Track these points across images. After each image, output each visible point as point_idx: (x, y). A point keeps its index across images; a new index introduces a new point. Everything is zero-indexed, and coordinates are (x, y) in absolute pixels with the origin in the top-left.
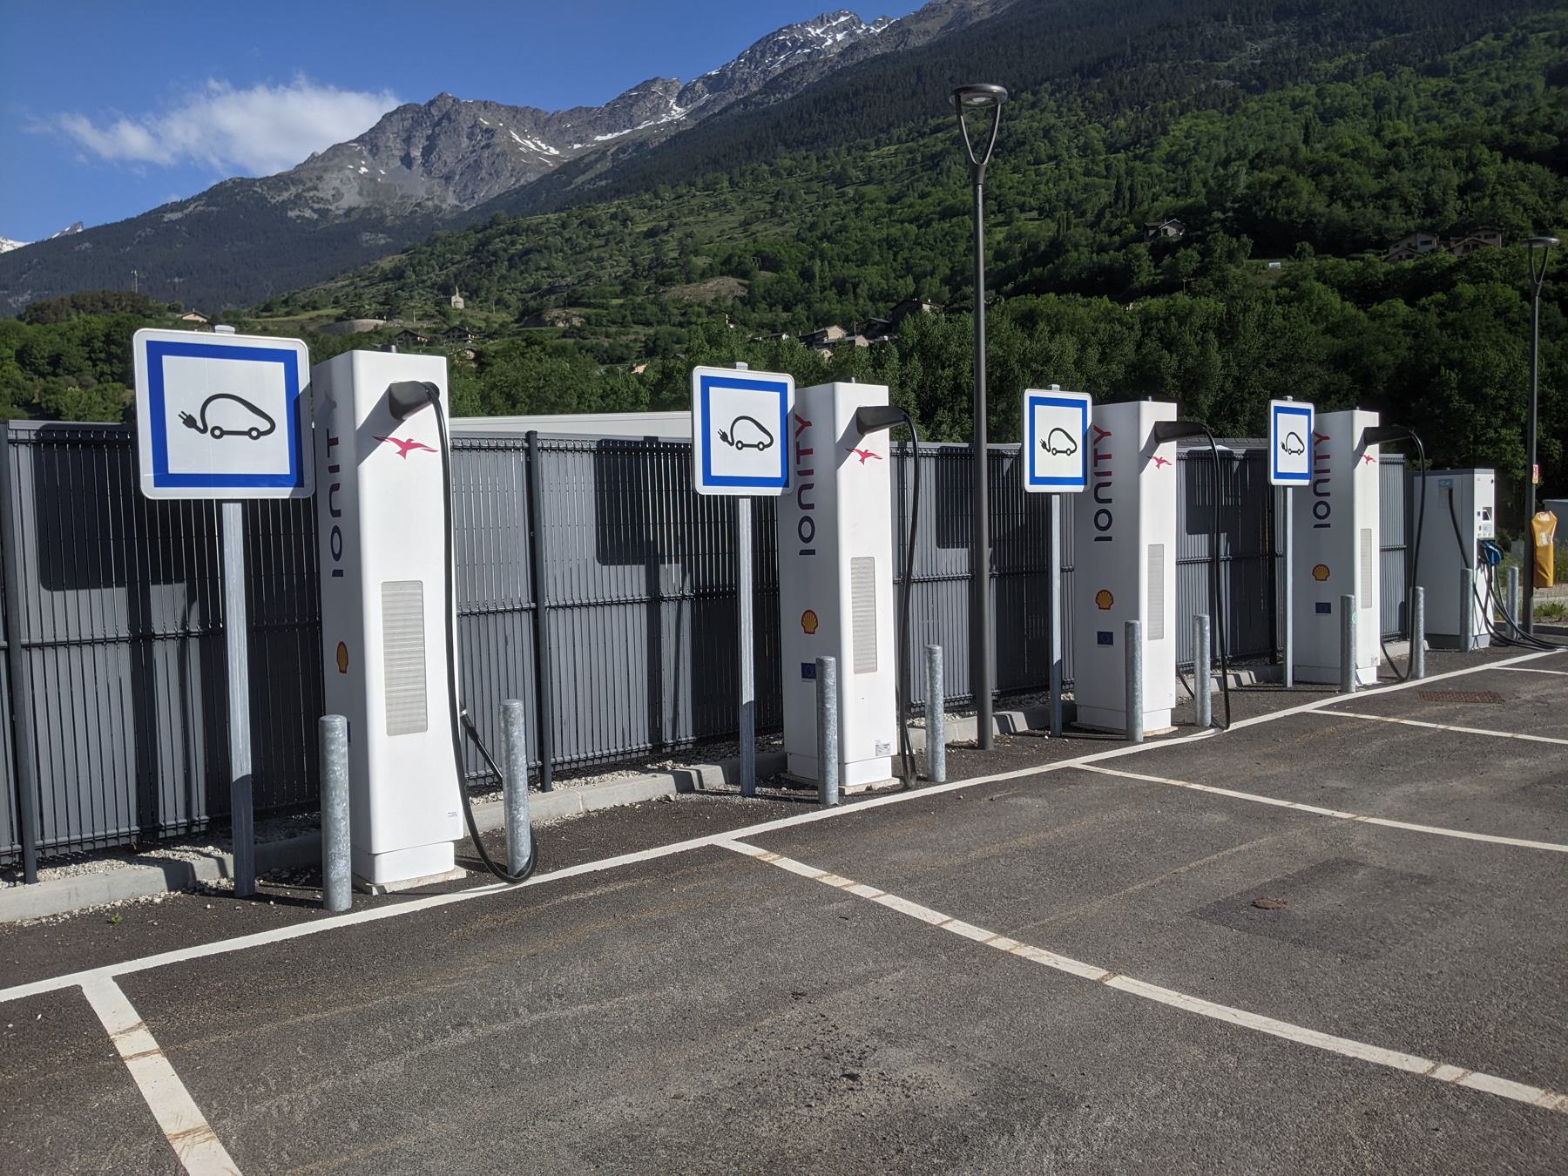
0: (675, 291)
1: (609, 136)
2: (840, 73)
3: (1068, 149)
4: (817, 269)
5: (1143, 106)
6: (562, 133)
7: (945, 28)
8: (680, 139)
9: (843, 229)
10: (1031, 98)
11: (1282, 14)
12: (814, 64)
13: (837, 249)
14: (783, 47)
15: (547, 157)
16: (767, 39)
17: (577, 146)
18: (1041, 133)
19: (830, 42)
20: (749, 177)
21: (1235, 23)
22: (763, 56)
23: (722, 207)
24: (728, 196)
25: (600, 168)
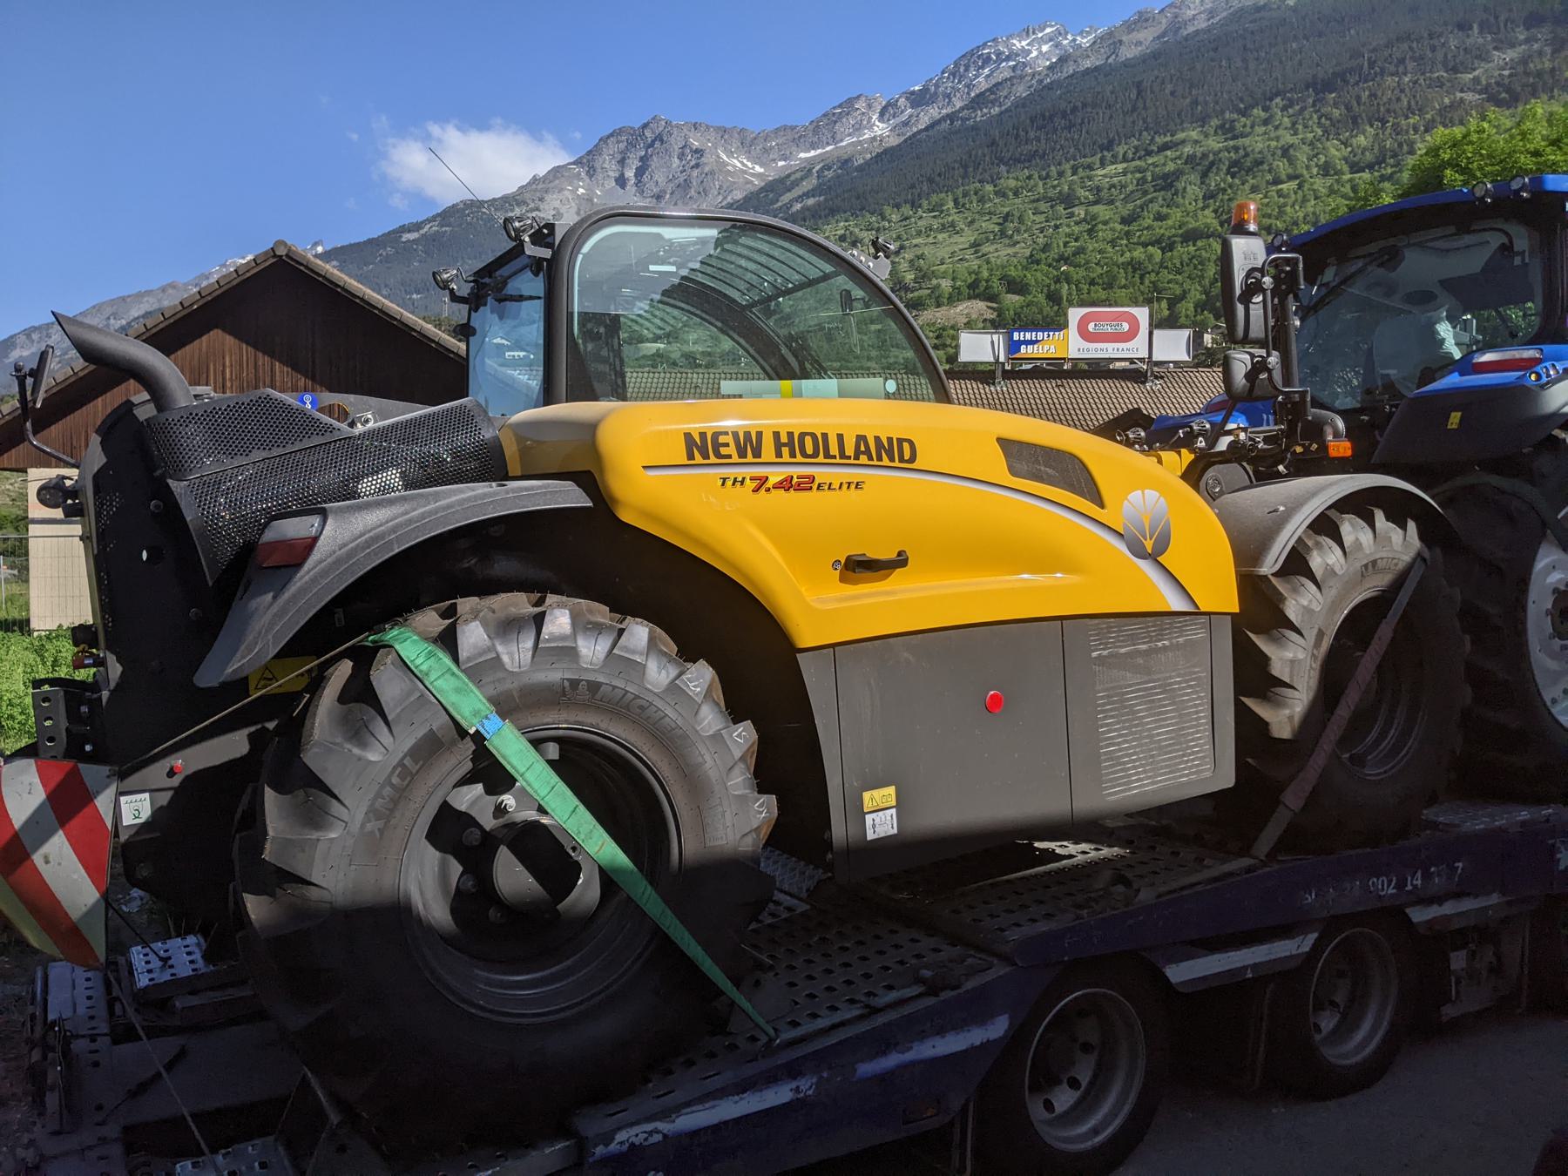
0: (928, 315)
1: (812, 153)
2: (1050, 87)
3: (1308, 168)
4: (1064, 292)
5: (1384, 122)
6: (766, 151)
7: (1158, 37)
8: (886, 157)
9: (1080, 251)
10: (1263, 115)
11: (1533, 20)
12: (1022, 77)
13: (1082, 272)
14: (987, 60)
15: (753, 175)
16: (972, 53)
17: (781, 163)
18: (1279, 152)
19: (1035, 54)
20: (974, 198)
21: (1481, 32)
22: (967, 70)
23: (951, 228)
24: (956, 217)
25: (807, 185)
